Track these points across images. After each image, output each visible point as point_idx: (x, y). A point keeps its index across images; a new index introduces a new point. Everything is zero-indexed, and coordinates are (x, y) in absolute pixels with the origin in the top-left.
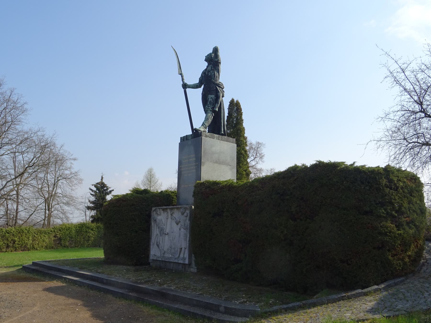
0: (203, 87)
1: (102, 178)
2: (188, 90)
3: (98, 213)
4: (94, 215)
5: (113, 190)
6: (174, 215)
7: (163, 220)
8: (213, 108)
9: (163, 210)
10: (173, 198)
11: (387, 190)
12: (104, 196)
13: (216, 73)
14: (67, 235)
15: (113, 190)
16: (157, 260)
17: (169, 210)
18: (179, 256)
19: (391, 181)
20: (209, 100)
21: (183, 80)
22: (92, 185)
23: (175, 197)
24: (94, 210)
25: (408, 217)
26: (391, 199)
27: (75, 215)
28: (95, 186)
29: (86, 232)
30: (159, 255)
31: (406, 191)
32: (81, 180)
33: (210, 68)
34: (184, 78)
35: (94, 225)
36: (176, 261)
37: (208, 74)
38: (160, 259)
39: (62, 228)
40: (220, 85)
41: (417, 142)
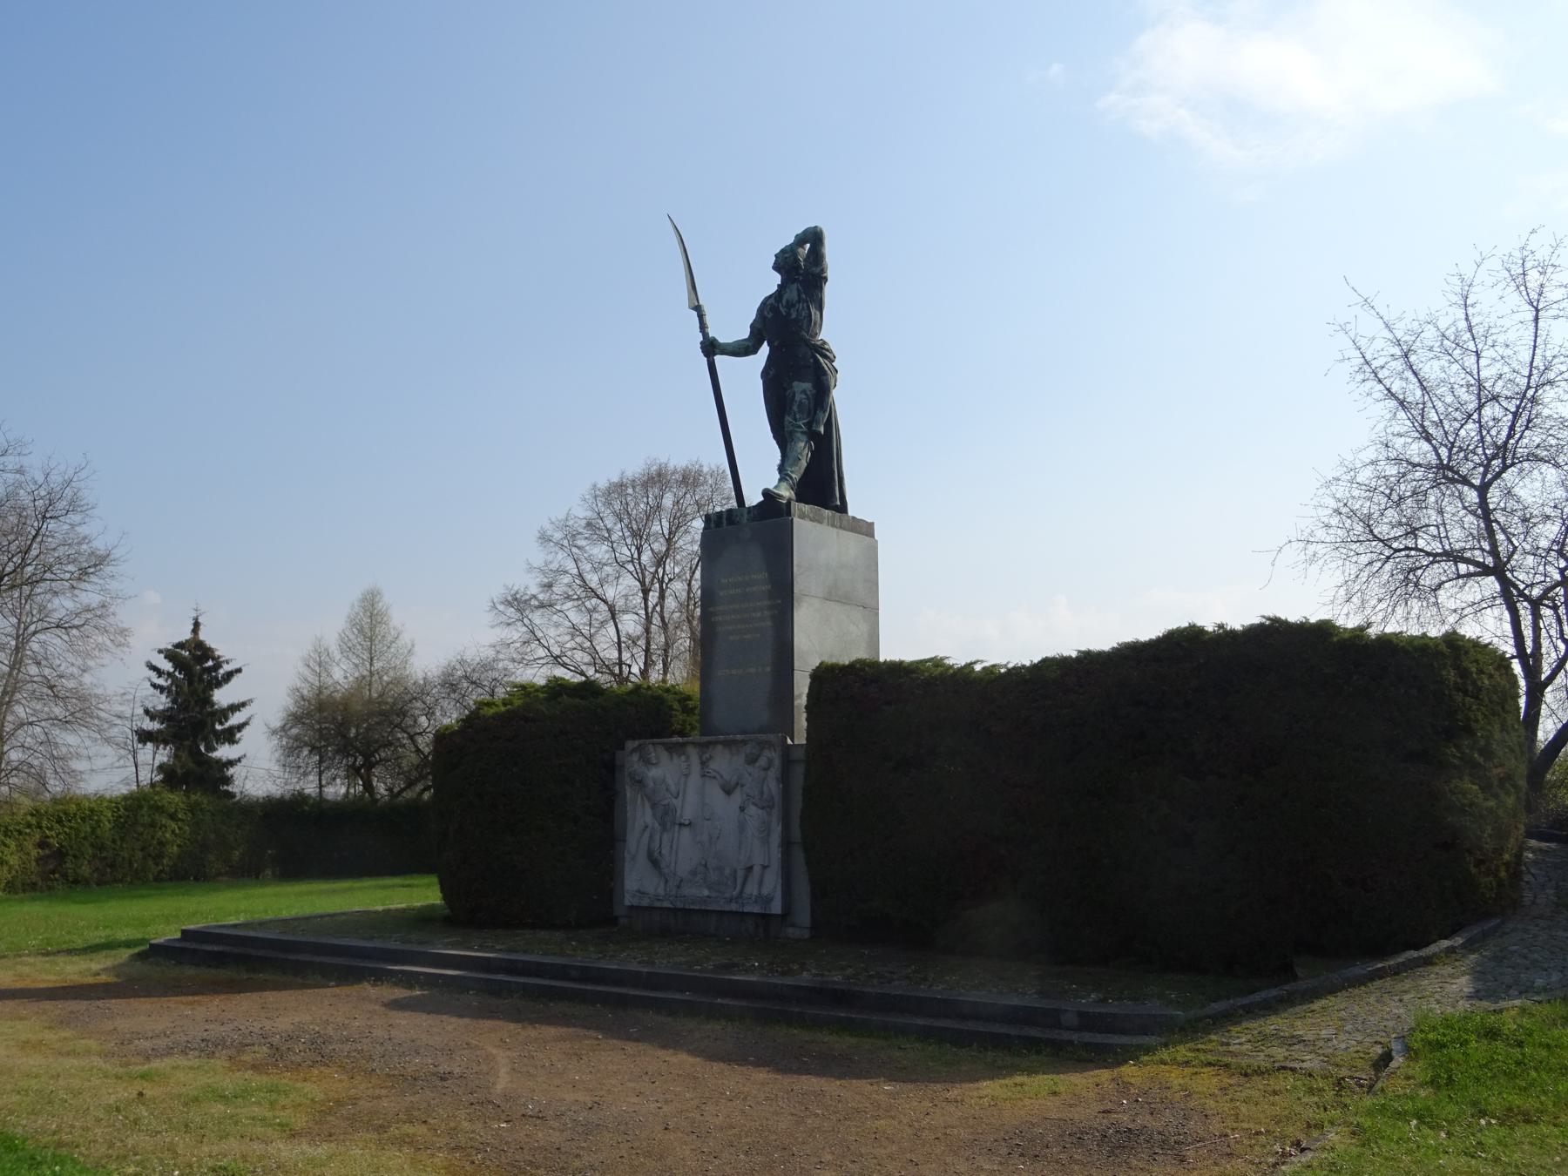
0: (765, 349)
1: (197, 625)
2: (718, 359)
3: (184, 755)
4: (165, 759)
5: (239, 671)
6: (713, 765)
7: (670, 781)
8: (809, 425)
9: (670, 749)
10: (671, 708)
11: (1459, 697)
12: (204, 692)
13: (813, 311)
14: (85, 838)
15: (239, 671)
16: (651, 909)
17: (693, 752)
18: (742, 892)
19: (1464, 673)
20: (797, 398)
21: (703, 327)
22: (160, 652)
23: (676, 706)
24: (166, 743)
25: (1501, 765)
26: (1468, 719)
27: (99, 763)
28: (170, 655)
29: (153, 825)
30: (661, 891)
31: (1495, 698)
32: (123, 632)
33: (795, 294)
34: (708, 319)
35: (174, 799)
36: (734, 907)
37: (789, 314)
38: (666, 904)
39: (66, 814)
40: (822, 350)
41: (1416, 549)
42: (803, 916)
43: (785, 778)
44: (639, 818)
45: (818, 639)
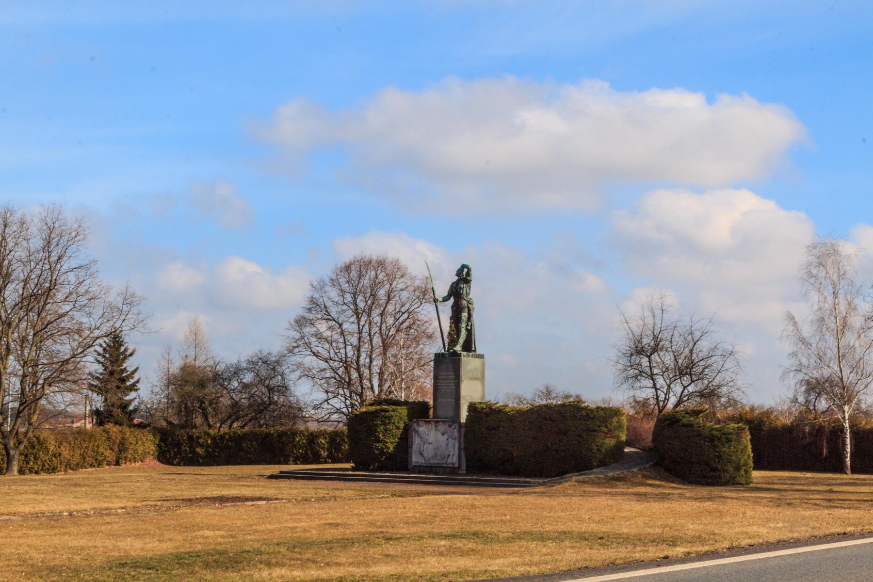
9: (426, 422)
42: (464, 467)
43: (459, 432)
44: (416, 441)
45: (471, 392)
